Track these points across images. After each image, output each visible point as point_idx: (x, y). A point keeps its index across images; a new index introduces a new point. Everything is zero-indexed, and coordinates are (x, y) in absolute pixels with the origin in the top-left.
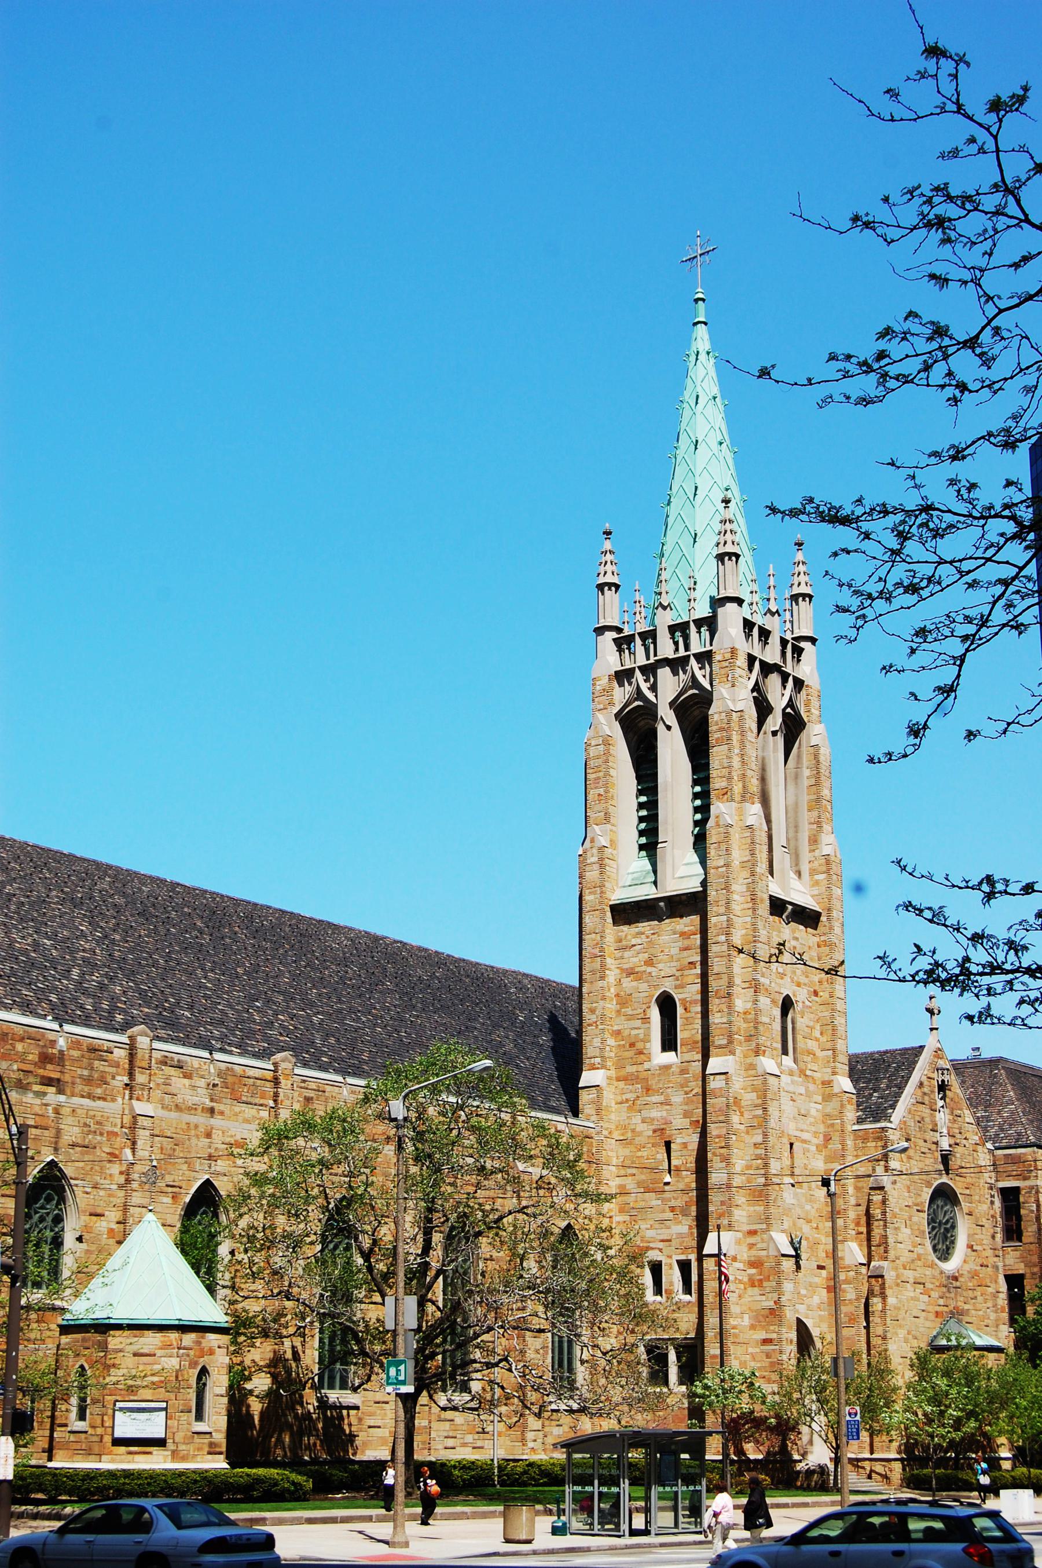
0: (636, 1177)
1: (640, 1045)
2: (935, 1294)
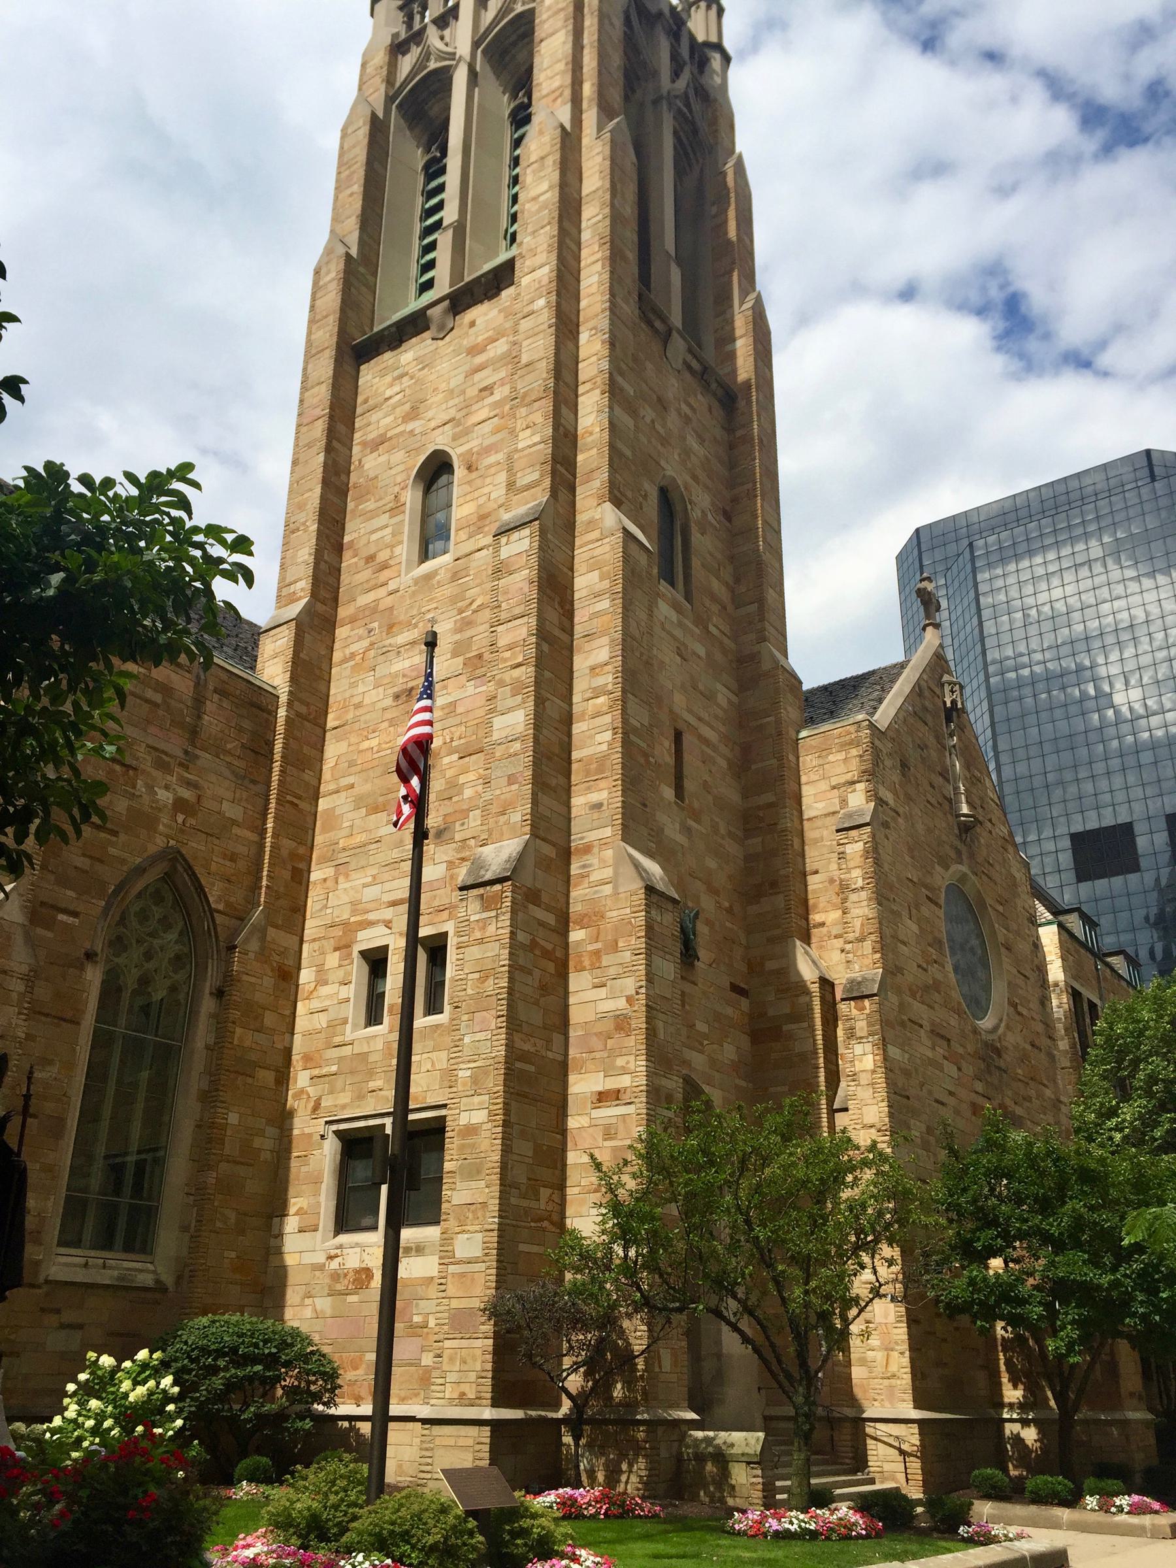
0: (356, 791)
1: (383, 556)
2: (969, 1070)
